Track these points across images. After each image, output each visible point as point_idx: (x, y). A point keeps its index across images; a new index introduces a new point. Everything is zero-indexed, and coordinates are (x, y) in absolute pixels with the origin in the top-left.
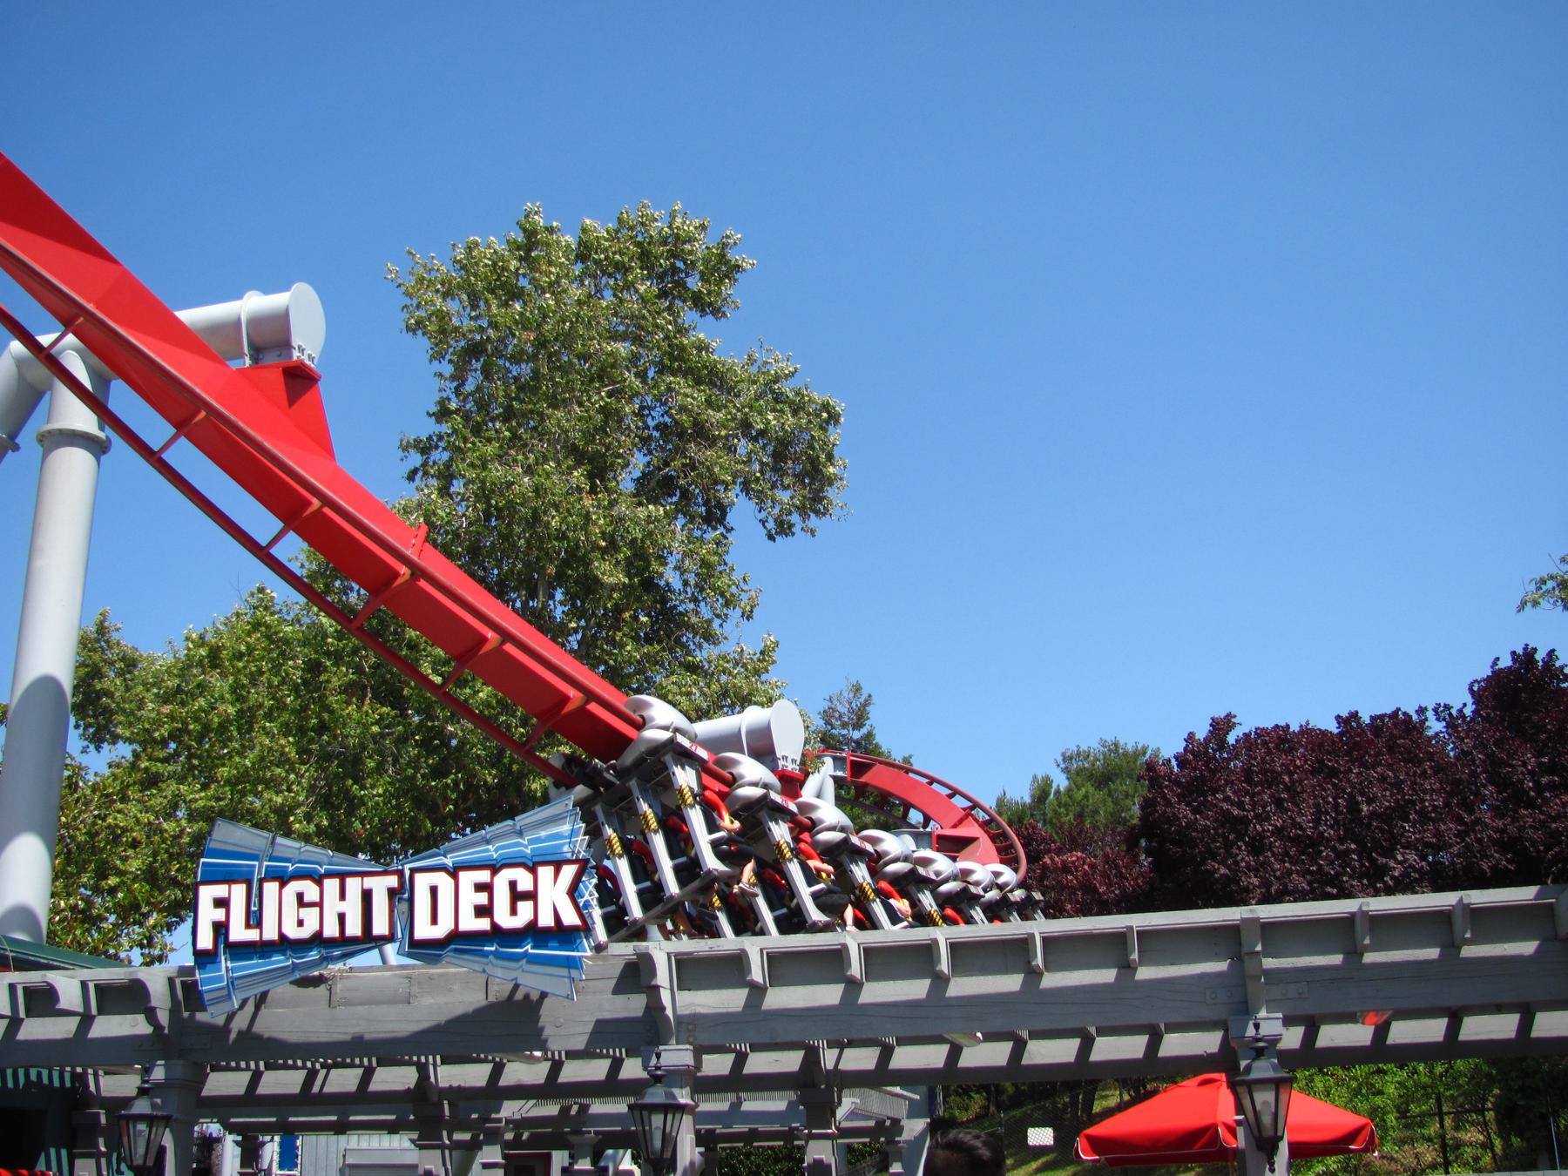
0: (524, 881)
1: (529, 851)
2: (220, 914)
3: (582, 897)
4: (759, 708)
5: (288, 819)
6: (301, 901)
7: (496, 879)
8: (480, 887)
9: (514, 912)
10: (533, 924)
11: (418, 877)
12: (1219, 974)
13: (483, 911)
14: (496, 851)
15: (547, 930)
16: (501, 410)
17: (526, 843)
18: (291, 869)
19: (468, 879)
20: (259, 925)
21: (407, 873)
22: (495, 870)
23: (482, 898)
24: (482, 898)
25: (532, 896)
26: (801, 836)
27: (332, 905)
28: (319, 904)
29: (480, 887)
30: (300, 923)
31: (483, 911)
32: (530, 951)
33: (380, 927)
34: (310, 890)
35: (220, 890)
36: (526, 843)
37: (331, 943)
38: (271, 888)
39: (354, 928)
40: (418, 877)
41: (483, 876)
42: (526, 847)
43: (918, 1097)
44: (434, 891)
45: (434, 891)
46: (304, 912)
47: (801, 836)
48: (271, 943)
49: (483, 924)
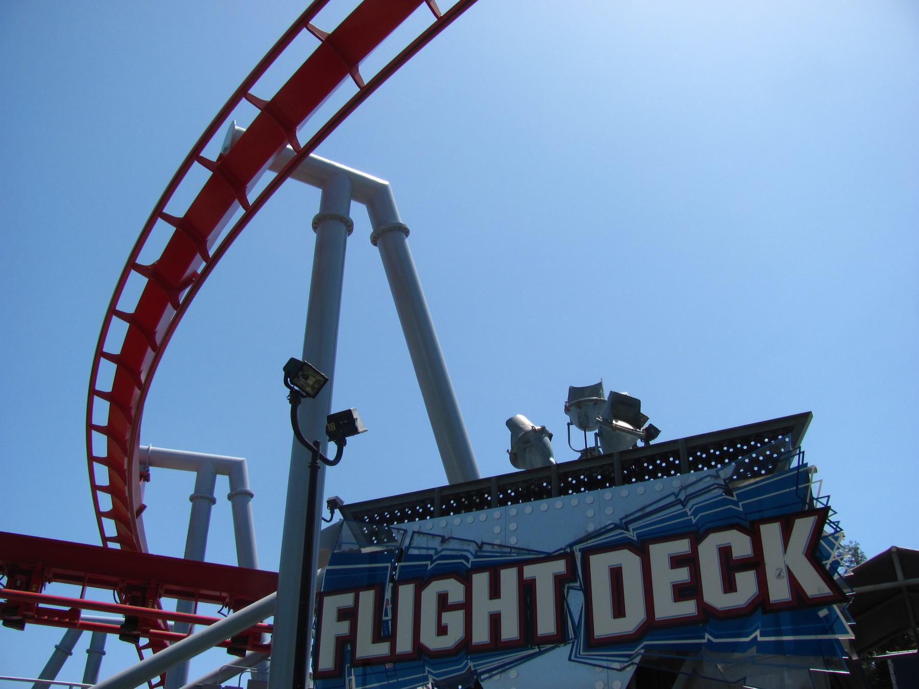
0: (741, 545)
1: (741, 509)
2: (344, 628)
3: (828, 558)
4: (252, 505)
5: (468, 502)
6: (443, 603)
7: (701, 548)
8: (676, 562)
9: (729, 586)
10: (761, 601)
11: (594, 559)
12: (824, 541)
13: (681, 592)
14: (695, 514)
15: (781, 607)
16: (126, 585)
17: (735, 499)
18: (429, 567)
19: (660, 553)
20: (392, 638)
21: (578, 555)
22: (697, 536)
23: (683, 575)
24: (683, 575)
25: (756, 563)
26: (337, 511)
27: (482, 606)
28: (467, 606)
29: (676, 562)
30: (442, 630)
31: (681, 592)
32: (760, 639)
33: (546, 624)
34: (454, 589)
35: (346, 600)
36: (735, 499)
37: (482, 651)
38: (406, 592)
39: (510, 630)
40: (594, 559)
41: (682, 546)
42: (736, 503)
43: (849, 673)
44: (616, 575)
45: (616, 575)
46: (447, 617)
47: (337, 511)
48: (405, 657)
49: (688, 608)
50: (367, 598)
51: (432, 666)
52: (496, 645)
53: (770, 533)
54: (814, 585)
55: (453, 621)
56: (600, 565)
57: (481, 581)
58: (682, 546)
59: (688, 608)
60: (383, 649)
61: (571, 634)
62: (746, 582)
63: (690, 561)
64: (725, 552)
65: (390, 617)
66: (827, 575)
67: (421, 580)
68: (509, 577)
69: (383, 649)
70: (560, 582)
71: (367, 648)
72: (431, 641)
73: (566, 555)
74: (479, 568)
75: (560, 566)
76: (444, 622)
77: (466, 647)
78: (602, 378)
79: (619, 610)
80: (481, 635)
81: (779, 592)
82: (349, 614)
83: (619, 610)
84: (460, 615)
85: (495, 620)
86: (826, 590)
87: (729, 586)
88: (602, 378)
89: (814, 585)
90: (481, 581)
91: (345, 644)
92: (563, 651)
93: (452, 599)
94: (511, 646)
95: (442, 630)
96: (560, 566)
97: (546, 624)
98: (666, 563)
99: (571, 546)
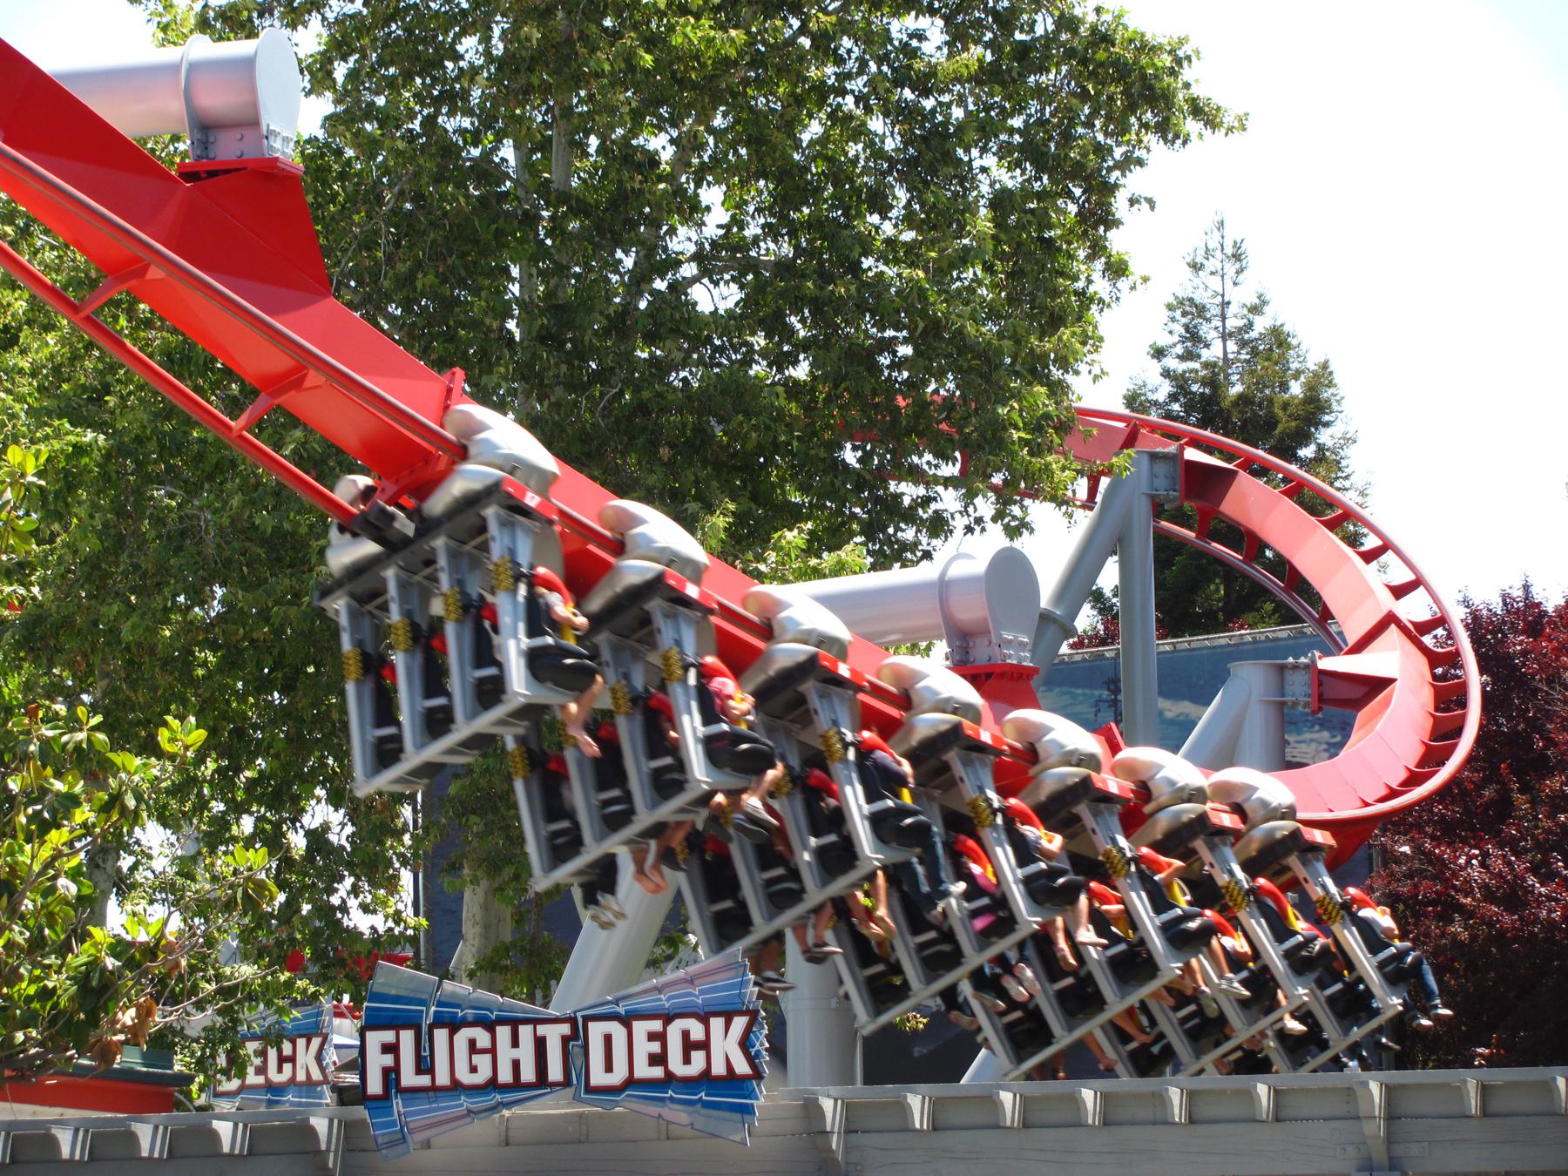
0: (697, 1032)
2: (388, 1060)
6: (473, 1047)
8: (652, 1037)
9: (687, 1060)
11: (591, 1025)
13: (658, 1059)
15: (719, 1078)
19: (641, 1028)
20: (431, 1071)
22: (668, 1019)
23: (655, 1047)
24: (655, 1047)
25: (705, 1045)
27: (505, 1053)
28: (493, 1051)
29: (652, 1037)
30: (473, 1069)
33: (555, 1072)
39: (528, 1074)
40: (591, 1025)
41: (656, 1026)
42: (697, 997)
44: (608, 1039)
45: (608, 1039)
46: (476, 1059)
49: (658, 1072)
50: (407, 1037)
51: (466, 1095)
52: (517, 1084)
53: (717, 1024)
54: (316, 1075)
55: (483, 1062)
56: (596, 1030)
57: (503, 1032)
58: (656, 1026)
59: (658, 1072)
60: (425, 1080)
61: (575, 1082)
62: (698, 1057)
63: (660, 1037)
64: (686, 1034)
65: (427, 1053)
66: (322, 1069)
67: (454, 1026)
68: (525, 1032)
69: (425, 1080)
70: (565, 1040)
71: (409, 1078)
72: (465, 1077)
73: (572, 1020)
74: (502, 1021)
75: (565, 1029)
76: (474, 1062)
77: (493, 1084)
78: (973, 558)
79: (609, 1068)
80: (505, 1076)
81: (719, 1069)
82: (391, 1049)
83: (609, 1068)
84: (488, 1057)
85: (516, 1065)
86: (321, 1078)
87: (687, 1060)
88: (973, 558)
89: (316, 1075)
90: (503, 1032)
91: (391, 1075)
92: (570, 1091)
93: (479, 1045)
94: (529, 1086)
95: (473, 1069)
96: (565, 1029)
97: (555, 1072)
98: (645, 1037)
99: (575, 1013)
